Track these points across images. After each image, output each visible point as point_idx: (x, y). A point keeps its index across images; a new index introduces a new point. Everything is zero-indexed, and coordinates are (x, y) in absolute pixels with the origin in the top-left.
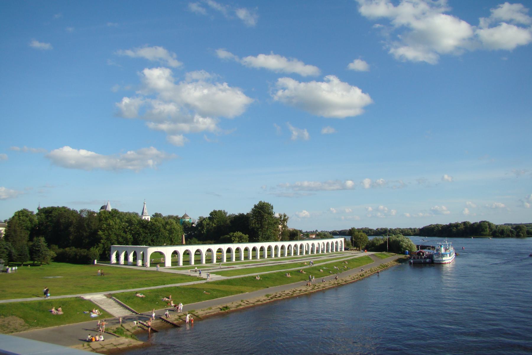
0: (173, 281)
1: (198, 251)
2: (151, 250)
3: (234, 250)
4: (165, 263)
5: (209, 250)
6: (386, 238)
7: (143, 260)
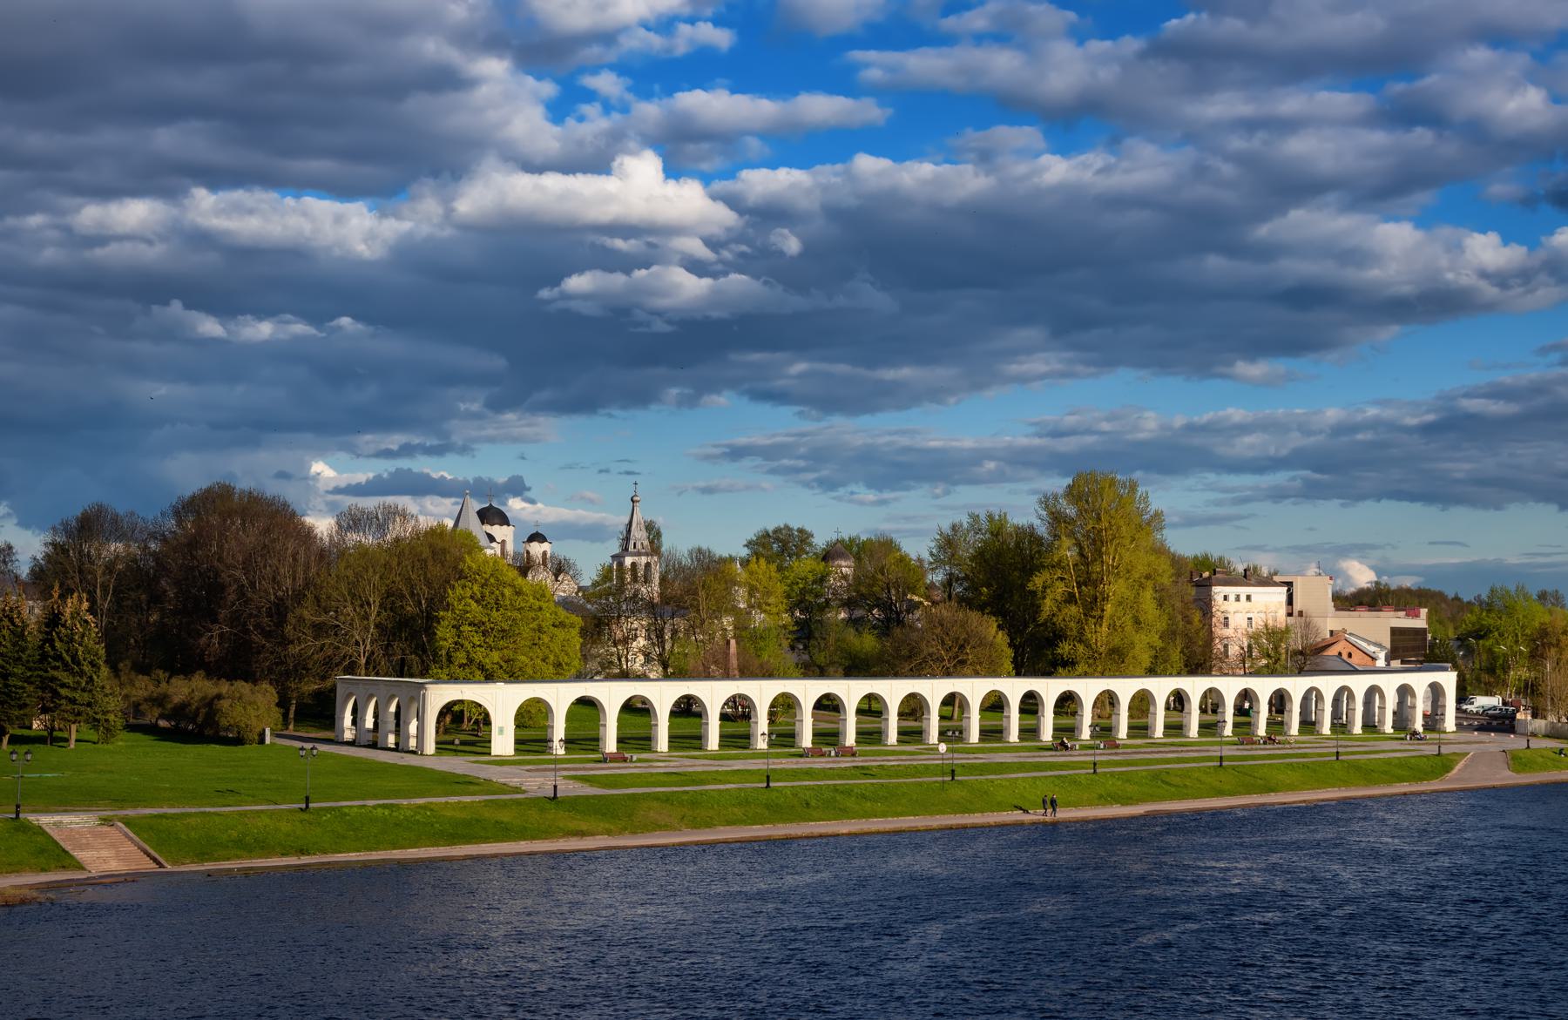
0: (702, 782)
1: (734, 701)
2: (439, 695)
3: (851, 704)
4: (597, 740)
5: (1246, 695)
6: (483, 433)
7: (397, 733)
